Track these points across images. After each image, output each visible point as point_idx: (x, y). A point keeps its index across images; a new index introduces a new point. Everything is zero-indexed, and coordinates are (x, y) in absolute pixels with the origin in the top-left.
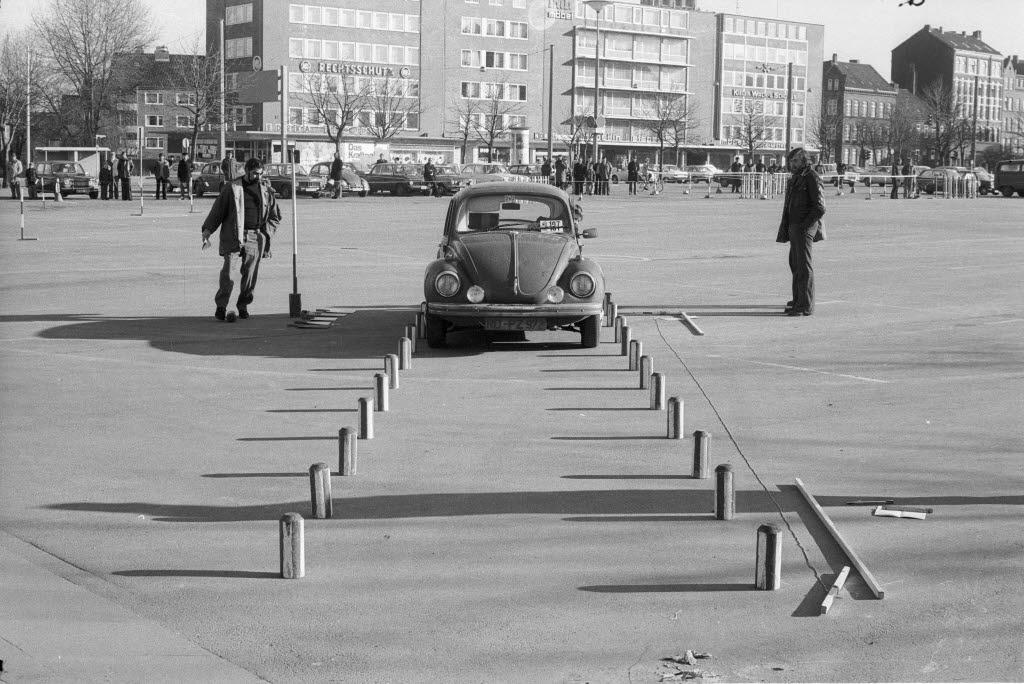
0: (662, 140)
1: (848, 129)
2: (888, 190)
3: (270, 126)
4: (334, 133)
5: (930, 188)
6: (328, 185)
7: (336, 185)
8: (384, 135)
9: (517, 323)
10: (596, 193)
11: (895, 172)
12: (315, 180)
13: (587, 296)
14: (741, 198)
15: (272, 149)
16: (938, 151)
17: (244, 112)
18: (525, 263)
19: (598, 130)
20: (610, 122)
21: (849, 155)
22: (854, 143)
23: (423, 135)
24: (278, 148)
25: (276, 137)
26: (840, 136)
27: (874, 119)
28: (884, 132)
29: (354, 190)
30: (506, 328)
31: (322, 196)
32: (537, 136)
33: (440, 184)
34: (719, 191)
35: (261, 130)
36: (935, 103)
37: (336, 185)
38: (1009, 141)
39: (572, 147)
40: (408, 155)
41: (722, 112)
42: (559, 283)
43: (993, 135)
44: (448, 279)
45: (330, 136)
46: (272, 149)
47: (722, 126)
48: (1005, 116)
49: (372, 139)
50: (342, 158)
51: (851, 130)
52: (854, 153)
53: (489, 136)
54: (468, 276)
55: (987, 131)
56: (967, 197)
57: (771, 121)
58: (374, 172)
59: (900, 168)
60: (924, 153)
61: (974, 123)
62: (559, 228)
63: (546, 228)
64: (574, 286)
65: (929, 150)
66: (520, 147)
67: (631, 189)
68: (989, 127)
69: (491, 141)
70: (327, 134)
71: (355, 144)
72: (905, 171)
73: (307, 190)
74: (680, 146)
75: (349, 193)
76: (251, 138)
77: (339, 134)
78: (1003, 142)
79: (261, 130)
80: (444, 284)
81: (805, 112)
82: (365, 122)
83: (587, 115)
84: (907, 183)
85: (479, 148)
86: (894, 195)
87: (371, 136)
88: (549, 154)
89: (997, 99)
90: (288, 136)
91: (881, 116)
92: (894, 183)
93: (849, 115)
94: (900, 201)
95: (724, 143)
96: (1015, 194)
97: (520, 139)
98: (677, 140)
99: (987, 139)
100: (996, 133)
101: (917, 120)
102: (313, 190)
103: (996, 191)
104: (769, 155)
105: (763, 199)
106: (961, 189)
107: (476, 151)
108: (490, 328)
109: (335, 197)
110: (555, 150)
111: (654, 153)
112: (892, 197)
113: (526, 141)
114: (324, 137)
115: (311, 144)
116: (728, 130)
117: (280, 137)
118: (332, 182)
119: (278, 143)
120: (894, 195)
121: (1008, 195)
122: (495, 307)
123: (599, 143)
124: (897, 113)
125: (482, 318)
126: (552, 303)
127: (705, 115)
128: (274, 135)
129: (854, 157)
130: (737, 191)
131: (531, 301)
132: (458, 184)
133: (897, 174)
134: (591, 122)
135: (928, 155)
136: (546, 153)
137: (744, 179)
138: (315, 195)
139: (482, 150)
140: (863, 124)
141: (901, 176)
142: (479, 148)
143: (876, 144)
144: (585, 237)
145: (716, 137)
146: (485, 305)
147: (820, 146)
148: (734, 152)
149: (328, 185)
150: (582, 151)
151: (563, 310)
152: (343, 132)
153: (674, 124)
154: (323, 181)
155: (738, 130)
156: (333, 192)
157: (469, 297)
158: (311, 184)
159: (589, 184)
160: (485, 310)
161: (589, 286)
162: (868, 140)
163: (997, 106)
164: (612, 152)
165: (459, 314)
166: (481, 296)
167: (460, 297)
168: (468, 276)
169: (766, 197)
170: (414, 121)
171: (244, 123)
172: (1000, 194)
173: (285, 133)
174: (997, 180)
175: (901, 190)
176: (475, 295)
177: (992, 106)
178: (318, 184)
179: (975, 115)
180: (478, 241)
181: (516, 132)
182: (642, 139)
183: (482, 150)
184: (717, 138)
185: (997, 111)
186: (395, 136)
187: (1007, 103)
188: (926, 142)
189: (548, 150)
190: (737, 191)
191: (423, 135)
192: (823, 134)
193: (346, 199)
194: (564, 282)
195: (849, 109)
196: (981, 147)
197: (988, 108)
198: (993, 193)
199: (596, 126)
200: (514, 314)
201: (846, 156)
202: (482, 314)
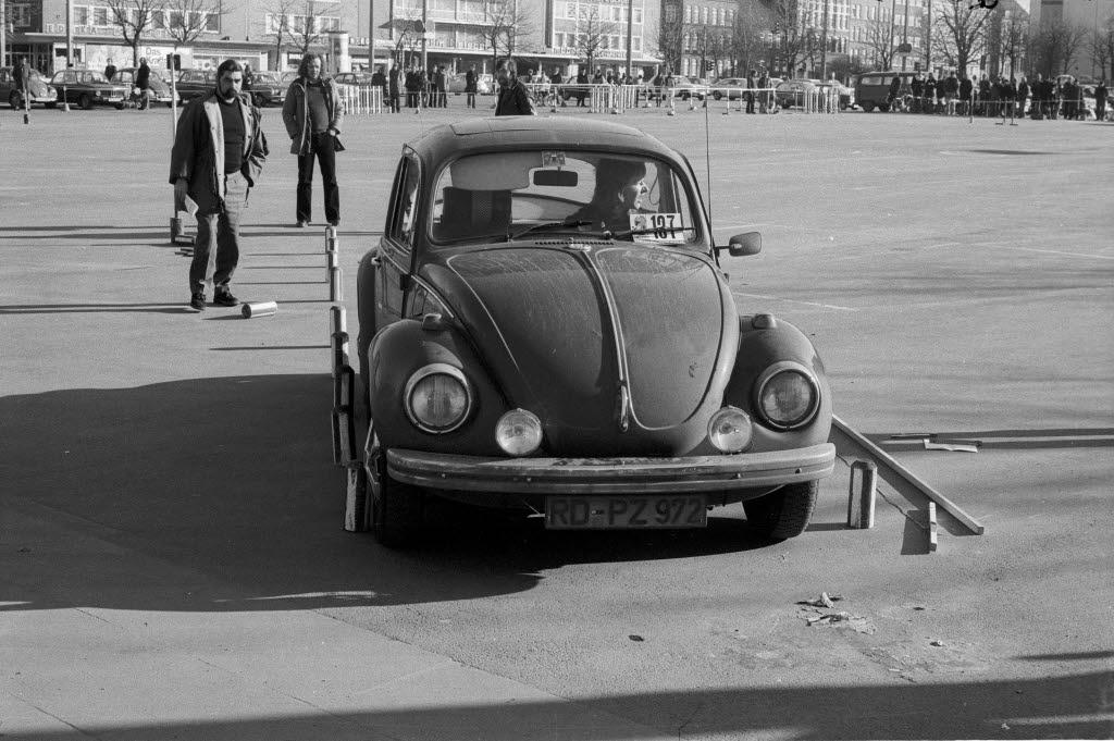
0: (495, 48)
1: (687, 37)
2: (743, 104)
3: (51, 27)
4: (130, 35)
5: (788, 102)
6: (133, 95)
7: (143, 94)
8: (185, 38)
9: (633, 509)
10: (430, 105)
11: (751, 85)
12: (116, 89)
13: (797, 426)
14: (590, 112)
15: (54, 52)
16: (783, 59)
17: (21, 12)
18: (640, 341)
19: (426, 35)
20: (441, 27)
21: (690, 66)
22: (695, 53)
23: (225, 39)
24: (62, 52)
25: (60, 39)
26: (679, 44)
27: (716, 27)
28: (725, 42)
29: (163, 100)
30: (603, 522)
31: (127, 107)
32: (352, 40)
33: (258, 94)
34: (563, 105)
35: (41, 31)
36: (784, 10)
37: (143, 94)
38: (856, 52)
39: (394, 54)
40: (208, 61)
41: (554, 17)
42: (730, 397)
43: (840, 45)
44: (439, 386)
45: (126, 39)
46: (54, 52)
47: (554, 32)
48: (852, 23)
49: (171, 42)
50: (149, 64)
51: (691, 40)
52: (694, 64)
53: (303, 40)
54: (498, 385)
55: (834, 41)
56: (829, 112)
57: (609, 28)
58: (183, 80)
59: (756, 80)
60: (768, 65)
61: (825, 32)
62: (673, 231)
63: (643, 232)
64: (770, 403)
65: (773, 60)
66: (338, 53)
67: (469, 100)
68: (836, 38)
69: (306, 47)
70: (123, 37)
71: (153, 48)
72: (762, 84)
73: (110, 100)
74: (513, 54)
75: (156, 104)
76: (29, 41)
77: (137, 36)
78: (851, 54)
79: (41, 31)
80: (430, 404)
81: (643, 19)
82: (160, 24)
83: (415, 18)
84: (763, 97)
85: (288, 53)
86: (750, 110)
87: (172, 39)
88: (371, 61)
89: (845, 6)
90: (75, 38)
91: (723, 23)
92: (749, 98)
93: (688, 22)
94: (758, 116)
95: (556, 52)
96: (877, 109)
97: (337, 44)
98: (510, 47)
99: (833, 51)
100: (843, 43)
101: (761, 28)
102: (118, 100)
103: (855, 106)
104: (604, 64)
105: (670, 114)
106: (821, 104)
107: (284, 57)
108: (559, 525)
109: (142, 108)
110: (377, 57)
111: (481, 61)
112: (748, 112)
113: (345, 46)
114: (119, 40)
115: (104, 48)
116: (560, 36)
117: (65, 40)
118: (138, 91)
119: (63, 46)
120: (750, 110)
121: (869, 110)
122: (575, 466)
123: (428, 49)
124: (740, 20)
125: (539, 501)
126: (721, 453)
127: (538, 19)
128: (56, 38)
129: (694, 68)
130: (583, 105)
131: (663, 448)
132: (279, 94)
133: (753, 87)
134: (418, 27)
135: (773, 65)
136: (367, 61)
137: (593, 91)
138: (119, 106)
139: (292, 56)
140: (703, 31)
141: (756, 89)
142: (288, 53)
143: (717, 53)
144: (734, 252)
145: (548, 44)
146: (546, 464)
147: (662, 55)
148: (568, 61)
149: (133, 95)
150: (407, 59)
151: (753, 471)
152: (141, 34)
153: (507, 29)
154: (128, 90)
155: (572, 37)
156: (140, 102)
157: (505, 442)
158: (114, 93)
159: (424, 95)
160: (548, 477)
161: (806, 396)
162: (709, 54)
163: (845, 14)
164: (438, 60)
165: (473, 485)
166: (534, 435)
167: (474, 437)
168: (498, 385)
169: (617, 111)
170: (213, 21)
171: (21, 23)
172: (861, 109)
173: (71, 35)
174: (858, 94)
175: (757, 105)
176: (517, 435)
177: (839, 13)
178: (122, 93)
179: (825, 23)
180: (500, 271)
181: (334, 36)
182: (466, 45)
183: (292, 56)
184: (549, 46)
185: (844, 19)
186: (198, 39)
187: (855, 11)
188: (772, 53)
189: (369, 56)
190: (583, 105)
191: (225, 39)
192: (663, 46)
193: (153, 110)
194: (744, 391)
195: (689, 15)
196: (829, 58)
197: (835, 16)
198: (853, 108)
199: (424, 31)
200: (625, 488)
201: (686, 67)
202: (540, 488)
